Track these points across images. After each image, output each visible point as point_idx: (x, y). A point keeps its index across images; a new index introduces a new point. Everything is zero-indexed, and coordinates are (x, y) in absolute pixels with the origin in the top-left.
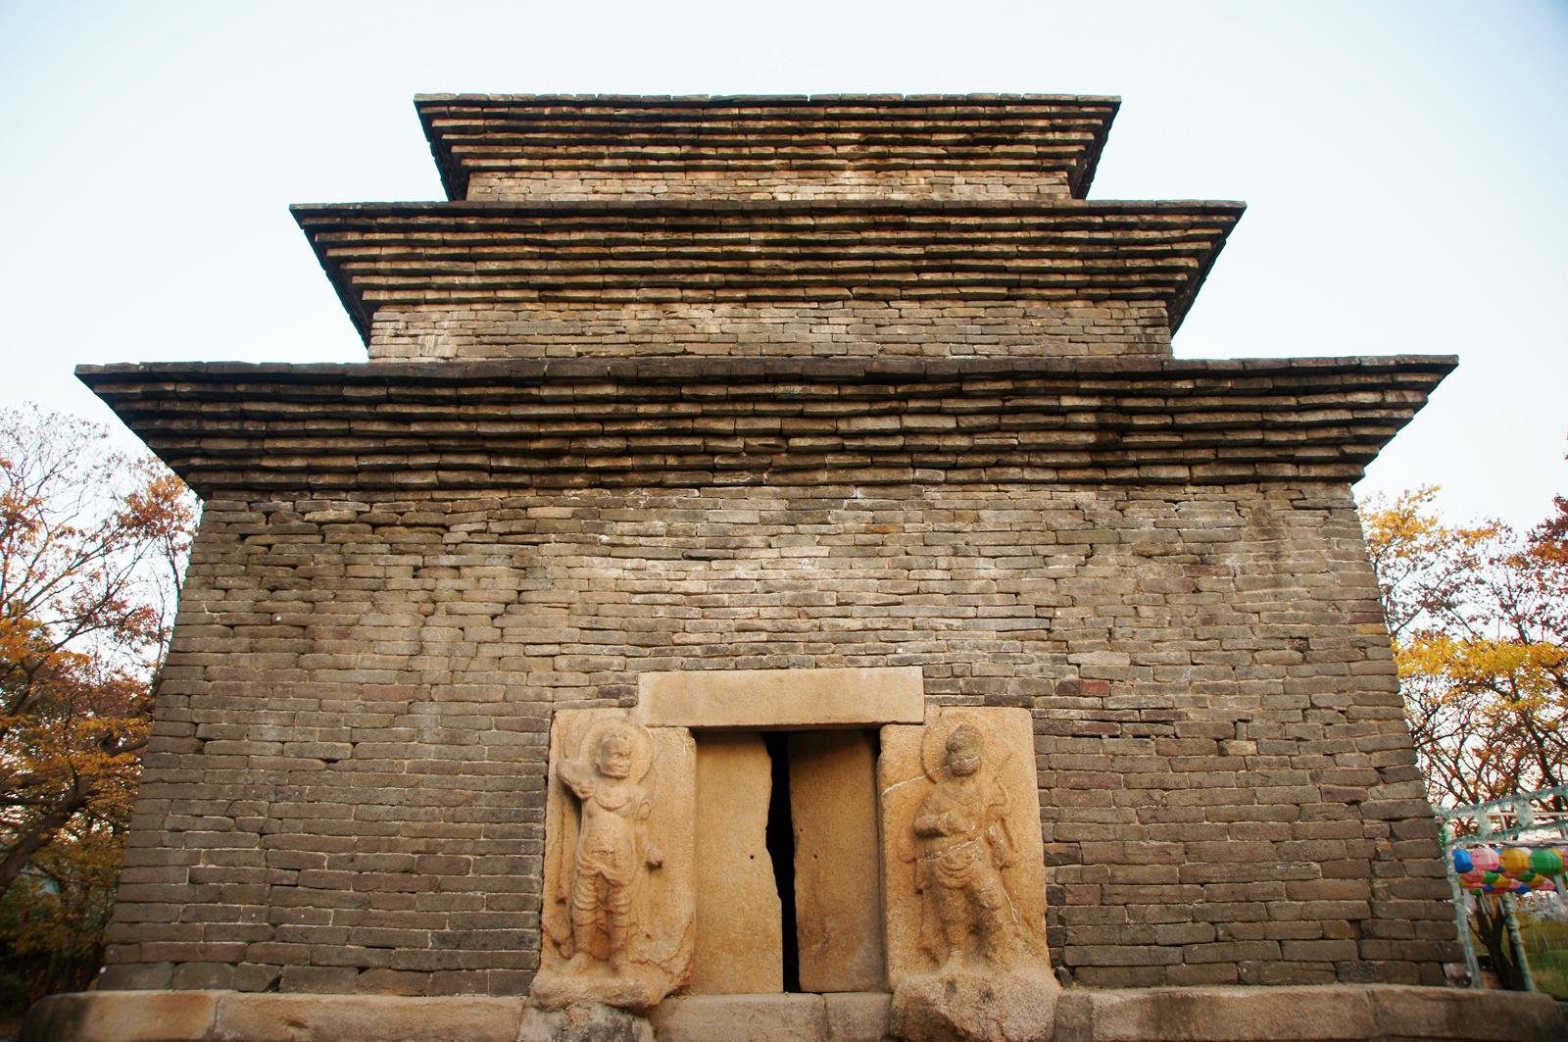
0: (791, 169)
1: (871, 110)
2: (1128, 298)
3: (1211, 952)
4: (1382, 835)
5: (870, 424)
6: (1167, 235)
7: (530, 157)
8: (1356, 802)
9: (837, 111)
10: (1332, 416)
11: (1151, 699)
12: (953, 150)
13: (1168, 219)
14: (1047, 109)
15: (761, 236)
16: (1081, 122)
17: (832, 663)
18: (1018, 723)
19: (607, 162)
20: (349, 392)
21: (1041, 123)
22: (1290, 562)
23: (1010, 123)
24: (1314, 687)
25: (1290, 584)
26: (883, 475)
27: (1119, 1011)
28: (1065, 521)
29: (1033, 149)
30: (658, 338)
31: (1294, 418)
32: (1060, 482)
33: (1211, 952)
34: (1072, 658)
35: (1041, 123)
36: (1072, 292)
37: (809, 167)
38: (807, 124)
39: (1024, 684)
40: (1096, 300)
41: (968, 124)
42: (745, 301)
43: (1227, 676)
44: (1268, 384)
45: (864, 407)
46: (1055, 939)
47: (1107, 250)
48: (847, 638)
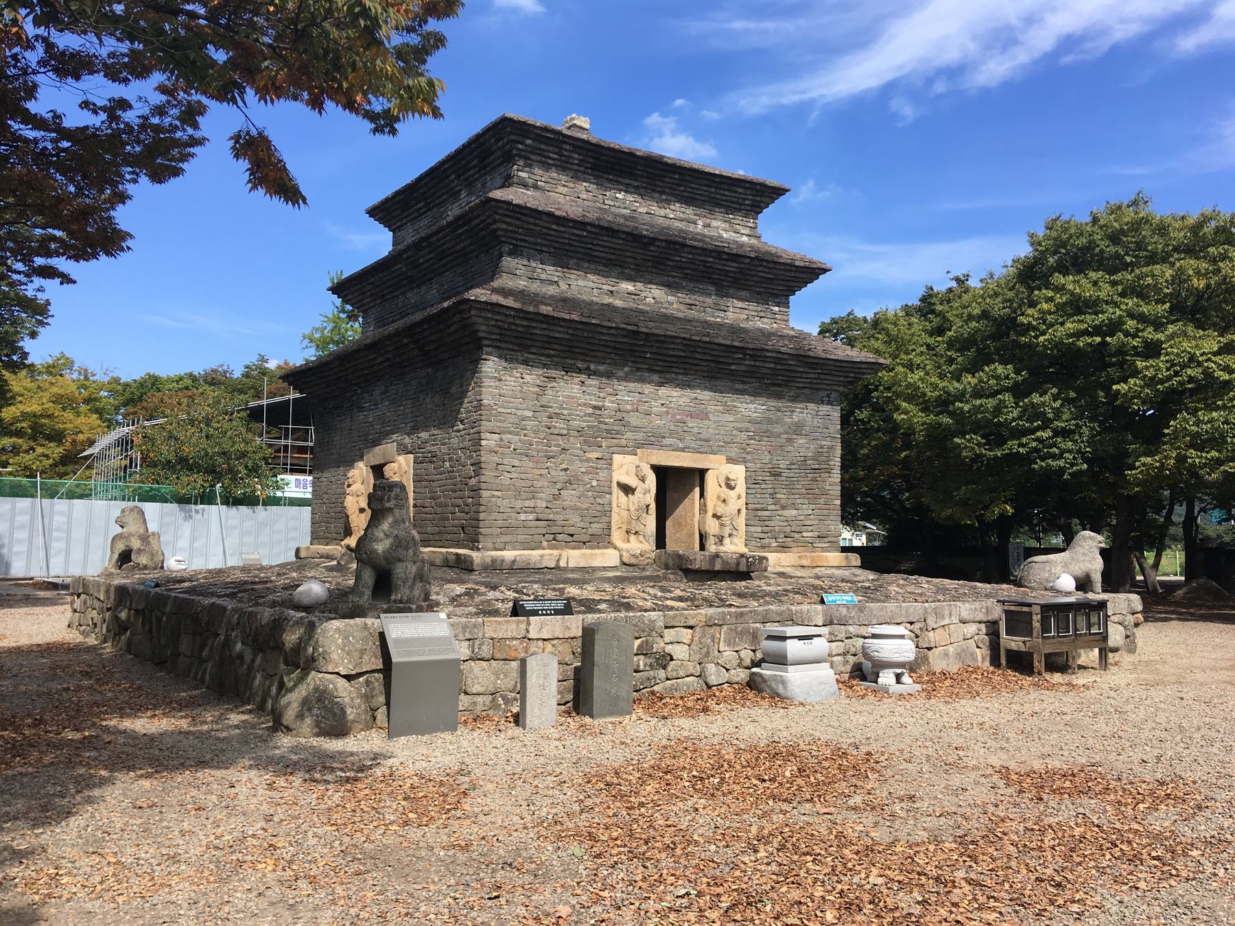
37: (455, 195)
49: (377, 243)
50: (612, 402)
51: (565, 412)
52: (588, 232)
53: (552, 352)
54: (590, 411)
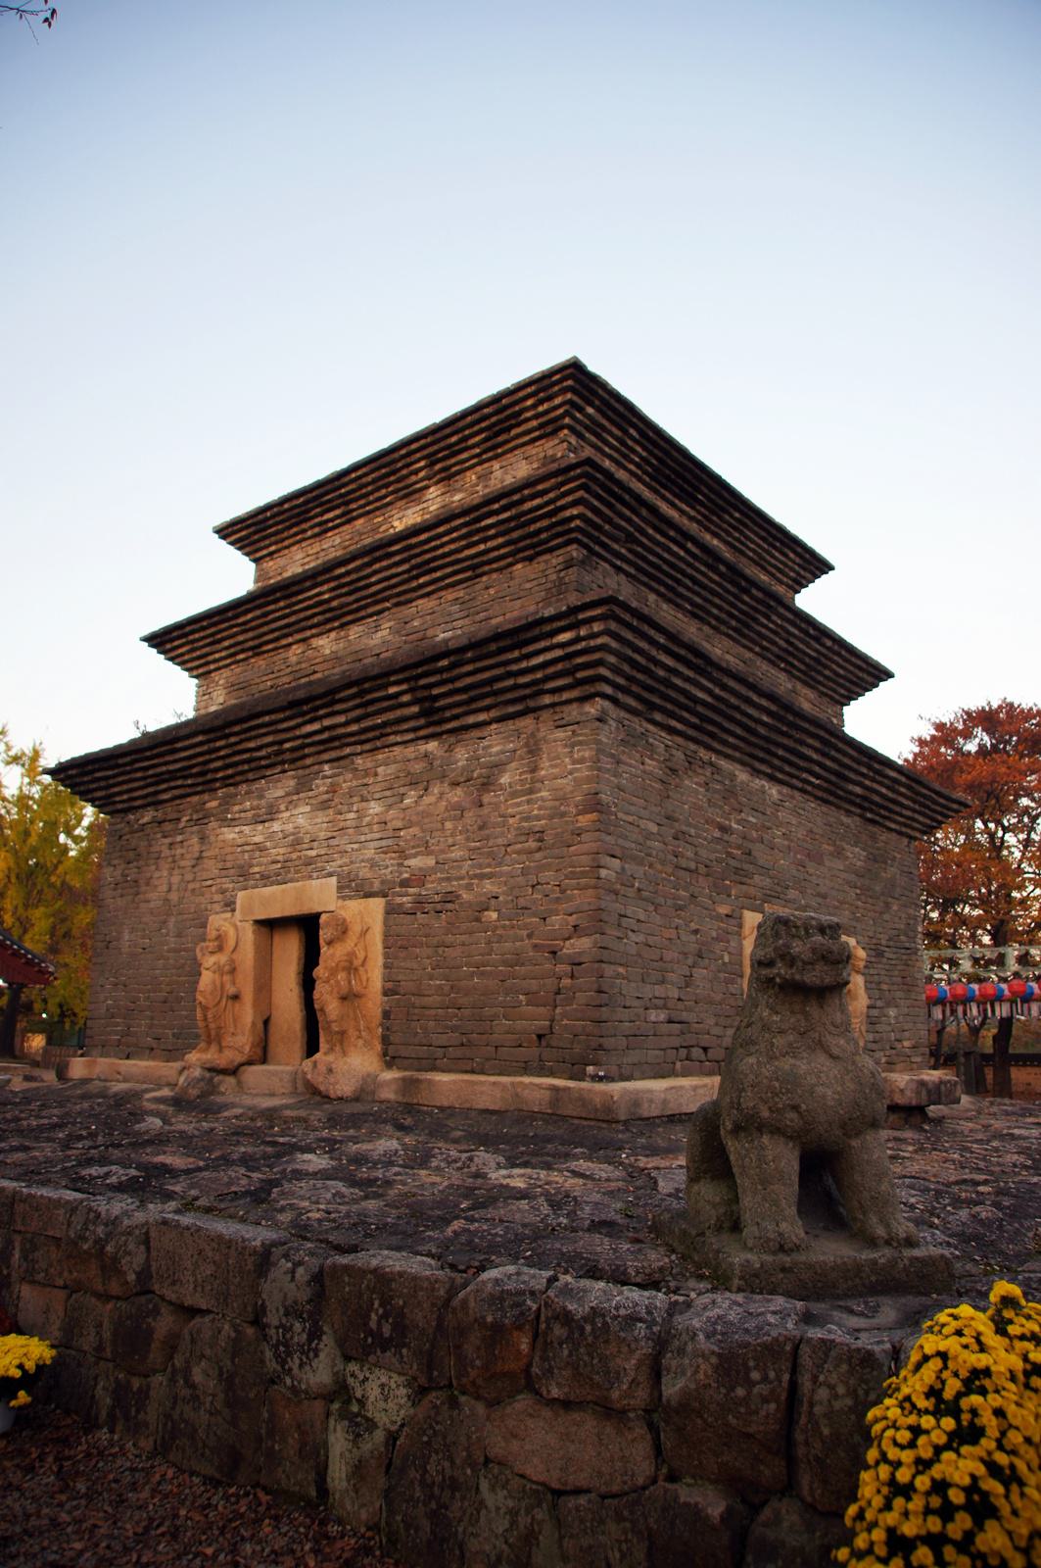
0: (402, 498)
1: (422, 442)
2: (551, 550)
3: (459, 1052)
4: (566, 975)
5: (309, 728)
6: (546, 498)
7: (276, 543)
8: (554, 953)
9: (403, 452)
10: (549, 656)
11: (446, 887)
12: (484, 446)
13: (540, 487)
14: (529, 390)
15: (325, 587)
16: (556, 388)
17: (303, 878)
18: (377, 905)
19: (309, 533)
20: (121, 761)
21: (529, 402)
22: (543, 773)
23: (509, 412)
24: (541, 868)
25: (540, 790)
26: (333, 754)
27: (387, 1083)
28: (418, 767)
29: (534, 423)
30: (303, 666)
31: (524, 664)
32: (418, 739)
33: (459, 1052)
34: (406, 863)
35: (529, 402)
36: (510, 560)
37: (411, 494)
38: (393, 467)
39: (383, 882)
40: (530, 559)
41: (483, 425)
42: (342, 626)
43: (489, 866)
44: (493, 647)
45: (300, 720)
46: (385, 1040)
47: (512, 524)
48: (309, 862)
49: (234, 576)
50: (738, 822)
51: (693, 831)
52: (687, 551)
53: (679, 726)
54: (717, 834)
